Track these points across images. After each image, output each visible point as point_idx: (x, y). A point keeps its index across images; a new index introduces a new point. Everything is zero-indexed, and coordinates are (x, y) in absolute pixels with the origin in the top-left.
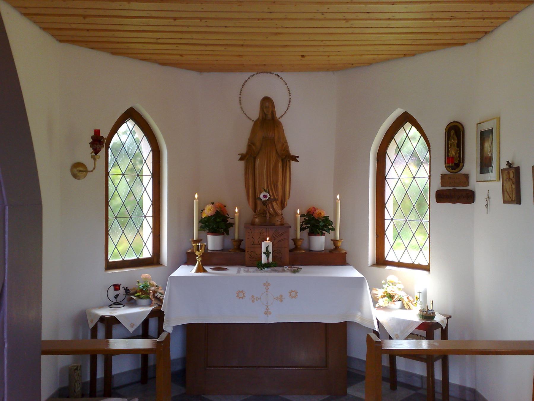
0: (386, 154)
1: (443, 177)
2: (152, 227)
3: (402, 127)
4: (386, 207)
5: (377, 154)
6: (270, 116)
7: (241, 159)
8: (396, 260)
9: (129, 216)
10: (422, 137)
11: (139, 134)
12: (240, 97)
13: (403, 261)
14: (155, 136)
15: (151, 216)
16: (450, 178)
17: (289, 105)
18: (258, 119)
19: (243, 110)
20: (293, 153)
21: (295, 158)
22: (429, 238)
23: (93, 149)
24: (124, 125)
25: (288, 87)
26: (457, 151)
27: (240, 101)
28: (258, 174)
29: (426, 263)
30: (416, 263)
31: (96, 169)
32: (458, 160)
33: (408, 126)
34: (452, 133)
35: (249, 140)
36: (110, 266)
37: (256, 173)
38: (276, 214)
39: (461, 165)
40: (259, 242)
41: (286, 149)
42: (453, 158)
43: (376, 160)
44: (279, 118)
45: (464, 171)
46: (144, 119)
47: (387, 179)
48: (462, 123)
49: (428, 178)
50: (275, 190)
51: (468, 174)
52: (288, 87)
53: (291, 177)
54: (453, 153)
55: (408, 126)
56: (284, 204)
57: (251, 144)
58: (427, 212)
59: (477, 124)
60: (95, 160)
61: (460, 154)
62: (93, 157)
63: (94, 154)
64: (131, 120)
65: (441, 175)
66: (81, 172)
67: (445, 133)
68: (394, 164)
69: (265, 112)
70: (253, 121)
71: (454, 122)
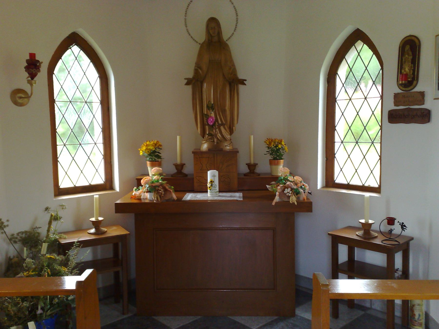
0: (337, 75)
1: (396, 96)
2: (103, 154)
3: (354, 46)
4: (336, 130)
5: (327, 75)
6: (216, 39)
7: (187, 84)
8: (345, 182)
9: (79, 143)
10: (374, 55)
11: (85, 60)
12: (185, 19)
13: (353, 183)
14: (102, 62)
15: (102, 143)
16: (404, 96)
17: (236, 26)
18: (205, 41)
19: (189, 33)
20: (241, 76)
21: (242, 82)
22: (380, 160)
23: (29, 73)
24: (69, 52)
25: (234, 6)
26: (411, 67)
27: (185, 23)
28: (205, 99)
29: (376, 185)
30: (366, 185)
31: (33, 94)
32: (412, 77)
33: (360, 45)
34: (408, 47)
35: (196, 64)
36: (60, 192)
37: (203, 98)
38: (225, 139)
39: (415, 82)
40: (207, 167)
41: (234, 71)
42: (406, 75)
43: (327, 81)
44: (227, 41)
45: (418, 89)
46: (90, 45)
47: (337, 101)
48: (418, 37)
49: (380, 98)
50: (223, 116)
51: (424, 92)
52: (234, 6)
53: (240, 101)
54: (407, 69)
55: (360, 45)
56: (233, 129)
57: (198, 67)
58: (379, 133)
59: (437, 36)
60: (31, 85)
61: (414, 71)
62: (29, 82)
63: (30, 79)
64: (76, 46)
65: (394, 94)
66: (22, 99)
67: (399, 48)
68: (346, 85)
69: (211, 33)
70: (200, 44)
71: (410, 36)
